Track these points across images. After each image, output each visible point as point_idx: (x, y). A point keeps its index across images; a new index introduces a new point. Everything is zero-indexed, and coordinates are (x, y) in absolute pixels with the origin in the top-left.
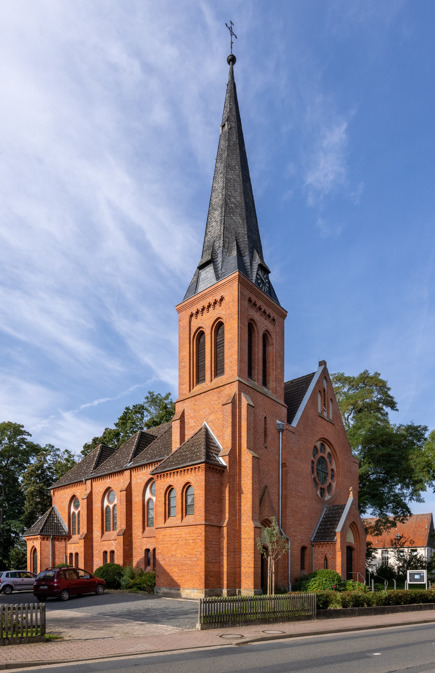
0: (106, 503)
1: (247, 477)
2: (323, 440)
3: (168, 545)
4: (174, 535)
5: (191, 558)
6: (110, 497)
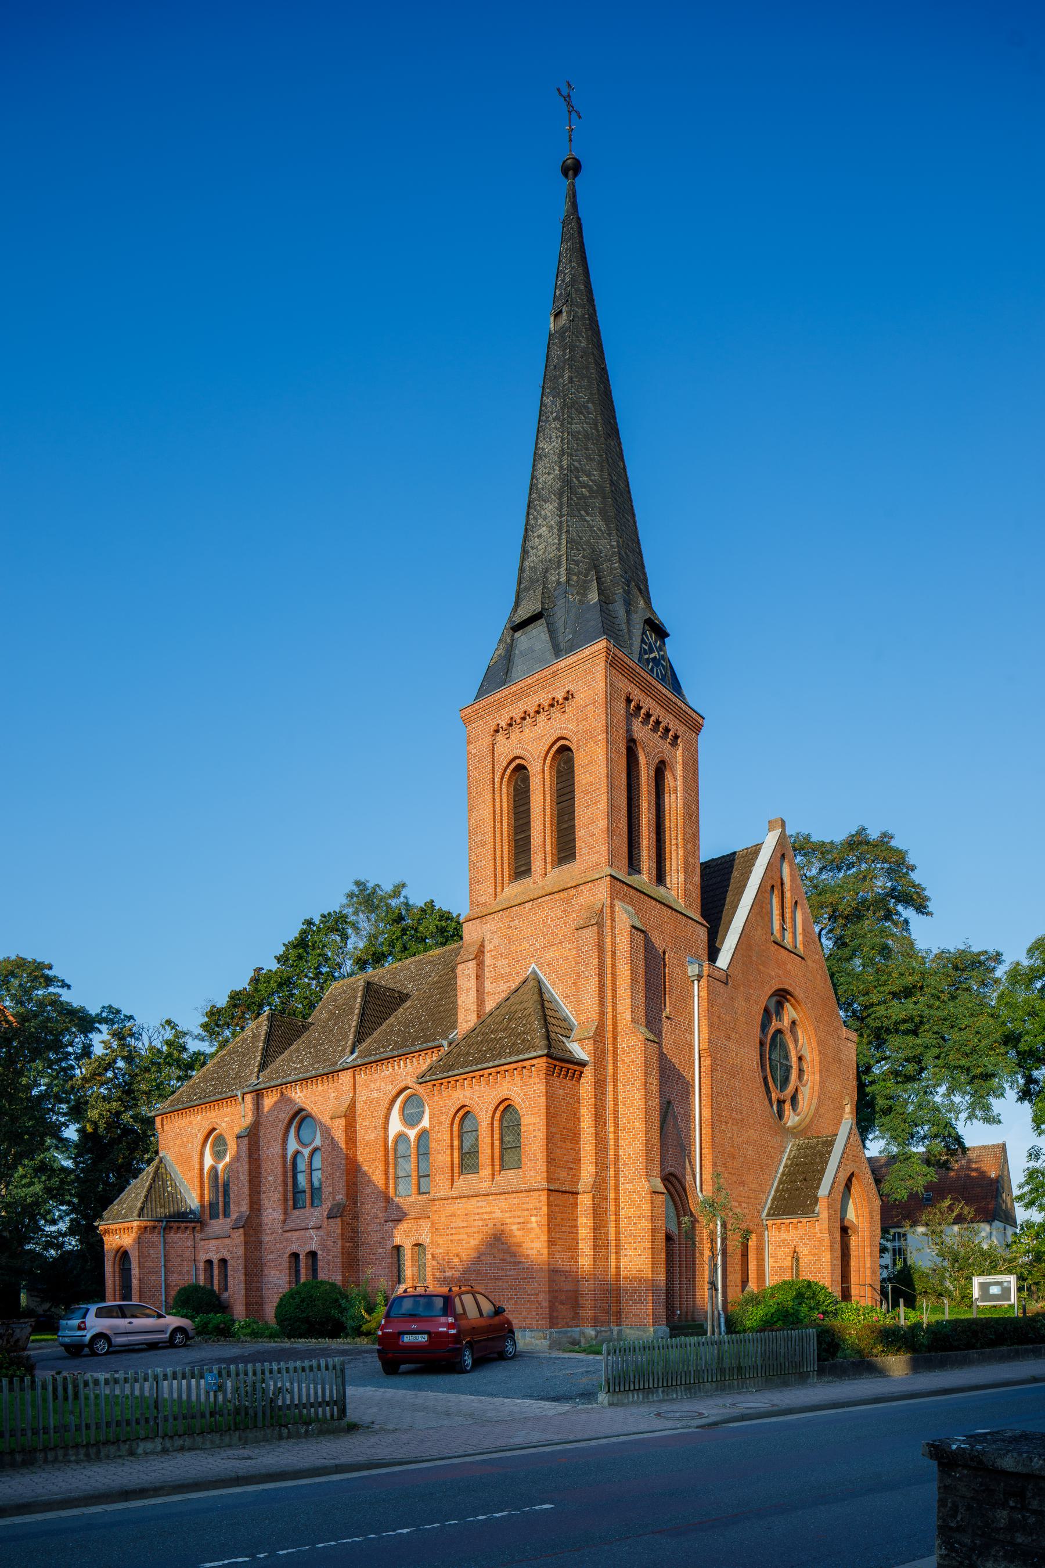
0: (293, 1145)
1: (633, 1084)
2: (782, 993)
4: (474, 1214)
6: (301, 1132)
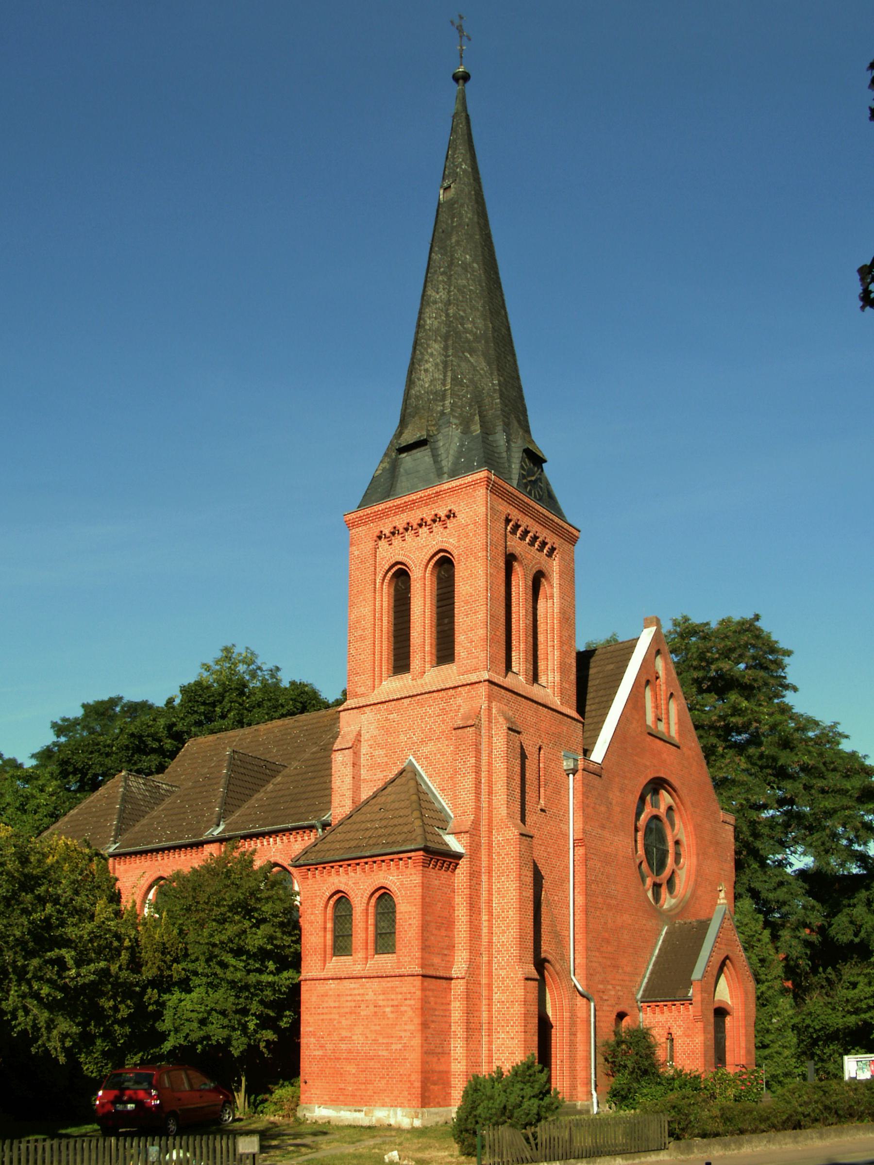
3: (332, 1016)
4: (347, 995)
5: (387, 1043)
